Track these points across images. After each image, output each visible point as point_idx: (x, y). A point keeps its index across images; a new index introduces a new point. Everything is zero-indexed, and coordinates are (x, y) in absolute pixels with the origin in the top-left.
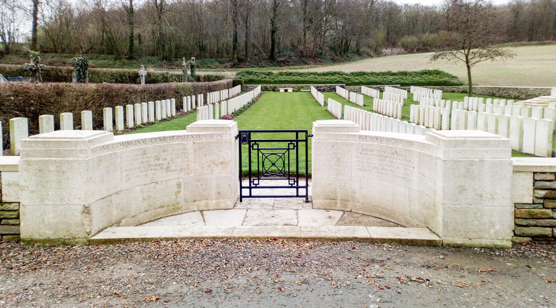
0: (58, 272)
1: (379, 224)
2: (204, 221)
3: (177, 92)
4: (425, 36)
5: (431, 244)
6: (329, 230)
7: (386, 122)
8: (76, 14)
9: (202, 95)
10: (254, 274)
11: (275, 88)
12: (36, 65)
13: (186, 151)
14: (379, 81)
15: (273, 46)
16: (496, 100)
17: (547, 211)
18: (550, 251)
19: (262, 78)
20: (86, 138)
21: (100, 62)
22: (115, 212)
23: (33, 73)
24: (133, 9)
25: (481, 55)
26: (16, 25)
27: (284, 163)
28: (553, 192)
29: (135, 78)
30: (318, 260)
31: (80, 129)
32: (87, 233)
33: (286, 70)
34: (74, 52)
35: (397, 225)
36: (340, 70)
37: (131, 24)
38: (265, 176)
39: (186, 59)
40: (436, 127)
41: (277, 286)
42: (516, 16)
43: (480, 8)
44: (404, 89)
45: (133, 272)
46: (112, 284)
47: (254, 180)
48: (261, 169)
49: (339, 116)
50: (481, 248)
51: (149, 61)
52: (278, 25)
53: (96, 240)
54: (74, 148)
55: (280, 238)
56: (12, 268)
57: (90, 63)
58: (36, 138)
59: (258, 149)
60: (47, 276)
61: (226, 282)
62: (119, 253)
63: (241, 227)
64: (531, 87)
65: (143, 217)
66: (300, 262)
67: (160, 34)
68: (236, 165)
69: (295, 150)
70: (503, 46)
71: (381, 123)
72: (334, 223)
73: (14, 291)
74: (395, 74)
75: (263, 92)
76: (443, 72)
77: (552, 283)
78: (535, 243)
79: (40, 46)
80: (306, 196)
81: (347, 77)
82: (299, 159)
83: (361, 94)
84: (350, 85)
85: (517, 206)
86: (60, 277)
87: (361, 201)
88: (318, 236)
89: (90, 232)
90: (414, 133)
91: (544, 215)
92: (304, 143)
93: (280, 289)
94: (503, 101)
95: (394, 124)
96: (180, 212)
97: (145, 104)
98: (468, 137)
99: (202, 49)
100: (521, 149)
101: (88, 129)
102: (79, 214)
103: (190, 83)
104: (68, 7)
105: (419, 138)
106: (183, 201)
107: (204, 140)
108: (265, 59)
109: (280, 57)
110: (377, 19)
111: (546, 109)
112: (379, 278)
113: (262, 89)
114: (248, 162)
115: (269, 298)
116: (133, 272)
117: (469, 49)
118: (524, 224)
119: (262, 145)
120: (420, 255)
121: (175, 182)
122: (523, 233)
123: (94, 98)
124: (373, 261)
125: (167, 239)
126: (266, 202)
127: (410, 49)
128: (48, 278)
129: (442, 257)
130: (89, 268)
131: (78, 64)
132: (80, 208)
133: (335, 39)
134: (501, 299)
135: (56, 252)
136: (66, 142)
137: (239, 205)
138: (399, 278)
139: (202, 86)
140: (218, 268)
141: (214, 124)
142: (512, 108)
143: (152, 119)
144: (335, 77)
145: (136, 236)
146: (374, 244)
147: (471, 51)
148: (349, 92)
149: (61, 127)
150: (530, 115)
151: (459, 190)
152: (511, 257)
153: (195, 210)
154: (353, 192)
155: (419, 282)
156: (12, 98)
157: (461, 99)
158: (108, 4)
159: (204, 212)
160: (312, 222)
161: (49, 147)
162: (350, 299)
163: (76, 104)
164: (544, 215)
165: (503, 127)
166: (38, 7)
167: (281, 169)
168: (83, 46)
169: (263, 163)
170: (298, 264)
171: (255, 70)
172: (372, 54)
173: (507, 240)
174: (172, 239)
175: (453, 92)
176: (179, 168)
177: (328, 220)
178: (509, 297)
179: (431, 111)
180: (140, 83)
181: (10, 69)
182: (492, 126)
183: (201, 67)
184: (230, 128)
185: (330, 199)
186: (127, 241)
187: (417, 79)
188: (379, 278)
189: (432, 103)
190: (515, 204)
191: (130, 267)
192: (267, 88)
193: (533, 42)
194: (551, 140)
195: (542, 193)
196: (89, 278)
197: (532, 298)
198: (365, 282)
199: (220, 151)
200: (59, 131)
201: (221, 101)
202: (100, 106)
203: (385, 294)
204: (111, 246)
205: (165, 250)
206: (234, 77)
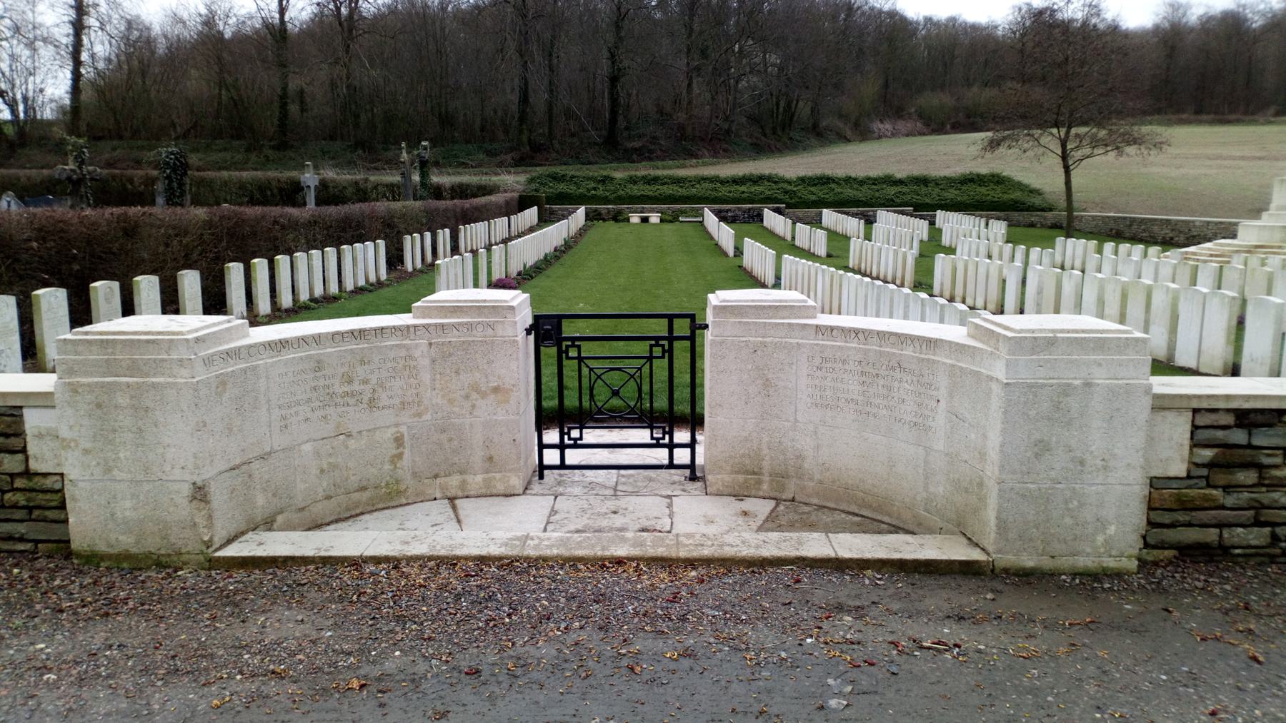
0: (153, 623)
1: (856, 528)
2: (459, 521)
3: (389, 225)
5: (967, 569)
6: (743, 542)
7: (879, 295)
8: (161, 48)
9: (447, 231)
10: (572, 637)
11: (620, 212)
12: (80, 168)
13: (412, 363)
14: (864, 198)
15: (614, 113)
16: (1124, 247)
17: (1214, 492)
18: (1212, 576)
19: (589, 191)
20: (189, 332)
21: (215, 157)
22: (260, 500)
23: (72, 187)
24: (285, 30)
25: (1095, 143)
26: (38, 81)
27: (640, 390)
28: (1228, 452)
29: (293, 193)
30: (717, 608)
31: (177, 312)
32: (204, 542)
33: (644, 170)
34: (157, 136)
35: (896, 529)
36: (774, 172)
37: (283, 65)
38: (597, 421)
39: (408, 146)
40: (991, 306)
41: (625, 662)
42: (1170, 56)
43: (1094, 34)
44: (921, 217)
45: (307, 628)
46: (265, 652)
47: (570, 429)
48: (586, 404)
49: (770, 280)
50: (1074, 575)
51: (324, 153)
52: (626, 63)
53: (224, 558)
54: (165, 357)
55: (631, 559)
56: (62, 611)
57: (193, 159)
58: (86, 333)
59: (580, 359)
60: (134, 631)
61: (511, 653)
62: (275, 587)
63: (542, 535)
65: (320, 510)
66: (675, 610)
67: (348, 87)
68: (527, 395)
69: (666, 360)
70: (1143, 124)
71: (866, 296)
72: (754, 526)
73: (70, 657)
74: (900, 182)
76: (1009, 179)
77: (1209, 642)
78: (1185, 562)
79: (88, 125)
80: (692, 466)
81: (789, 188)
82: (676, 381)
83: (822, 228)
84: (795, 206)
85: (1155, 483)
86: (156, 633)
87: (817, 476)
88: (716, 555)
89: (211, 540)
90: (942, 321)
91: (1207, 501)
92: (688, 343)
93: (632, 669)
95: (895, 300)
96: (404, 501)
97: (315, 253)
98: (1062, 331)
99: (447, 120)
100: (1171, 357)
101: (194, 312)
102: (185, 502)
103: (418, 203)
104: (145, 34)
105: (954, 332)
106: (409, 476)
107: (453, 337)
109: (630, 138)
110: (860, 50)
111: (1225, 270)
112: (852, 643)
113: (587, 215)
114: (556, 388)
115: (607, 687)
116: (307, 628)
117: (1070, 128)
118: (1167, 521)
119: (588, 349)
120: (944, 594)
121: (389, 434)
122: (1163, 542)
123: (204, 242)
124: (840, 608)
125: (377, 560)
126: (600, 480)
127: (937, 125)
128: (133, 633)
129: (990, 596)
130: (214, 618)
131: (168, 163)
132: (186, 490)
133: (761, 96)
134: (1106, 679)
135: (143, 582)
136: (148, 341)
137: (536, 487)
138: (895, 644)
139: (446, 210)
140: (491, 624)
141: (477, 299)
142: (1157, 265)
143: (334, 289)
144: (761, 189)
145: (309, 553)
146: (843, 572)
147: (1074, 131)
148: (794, 223)
149: (137, 309)
150: (1194, 282)
151: (1036, 449)
152: (1134, 592)
153: (438, 496)
154: (798, 457)
155: (939, 651)
156: (35, 244)
157: (1048, 243)
158: (230, 22)
159: (457, 502)
160: (702, 523)
161: (113, 353)
162: (786, 689)
163: (164, 254)
164: (1207, 501)
165: (1135, 310)
166: (84, 37)
167: (632, 404)
168: (176, 120)
169: (591, 389)
170: (670, 615)
171: (570, 170)
172: (849, 133)
173: (1129, 557)
174: (387, 559)
175: (1032, 225)
176: (397, 401)
177: (741, 520)
178: (1122, 674)
179: (982, 270)
180: (305, 204)
181: (29, 178)
182: (1113, 306)
183: (444, 166)
184: (512, 308)
185: (747, 472)
186: (289, 563)
187: (952, 194)
188: (852, 643)
189: (983, 251)
190: (1151, 479)
191: (299, 618)
192: (600, 214)
193: (1204, 117)
194: (1233, 337)
195: (1207, 454)
196: (215, 638)
197: (1165, 674)
198: (821, 653)
199: (490, 362)
200: (132, 317)
201: (491, 245)
202: (217, 258)
203: (864, 677)
204: (257, 572)
205: (374, 583)
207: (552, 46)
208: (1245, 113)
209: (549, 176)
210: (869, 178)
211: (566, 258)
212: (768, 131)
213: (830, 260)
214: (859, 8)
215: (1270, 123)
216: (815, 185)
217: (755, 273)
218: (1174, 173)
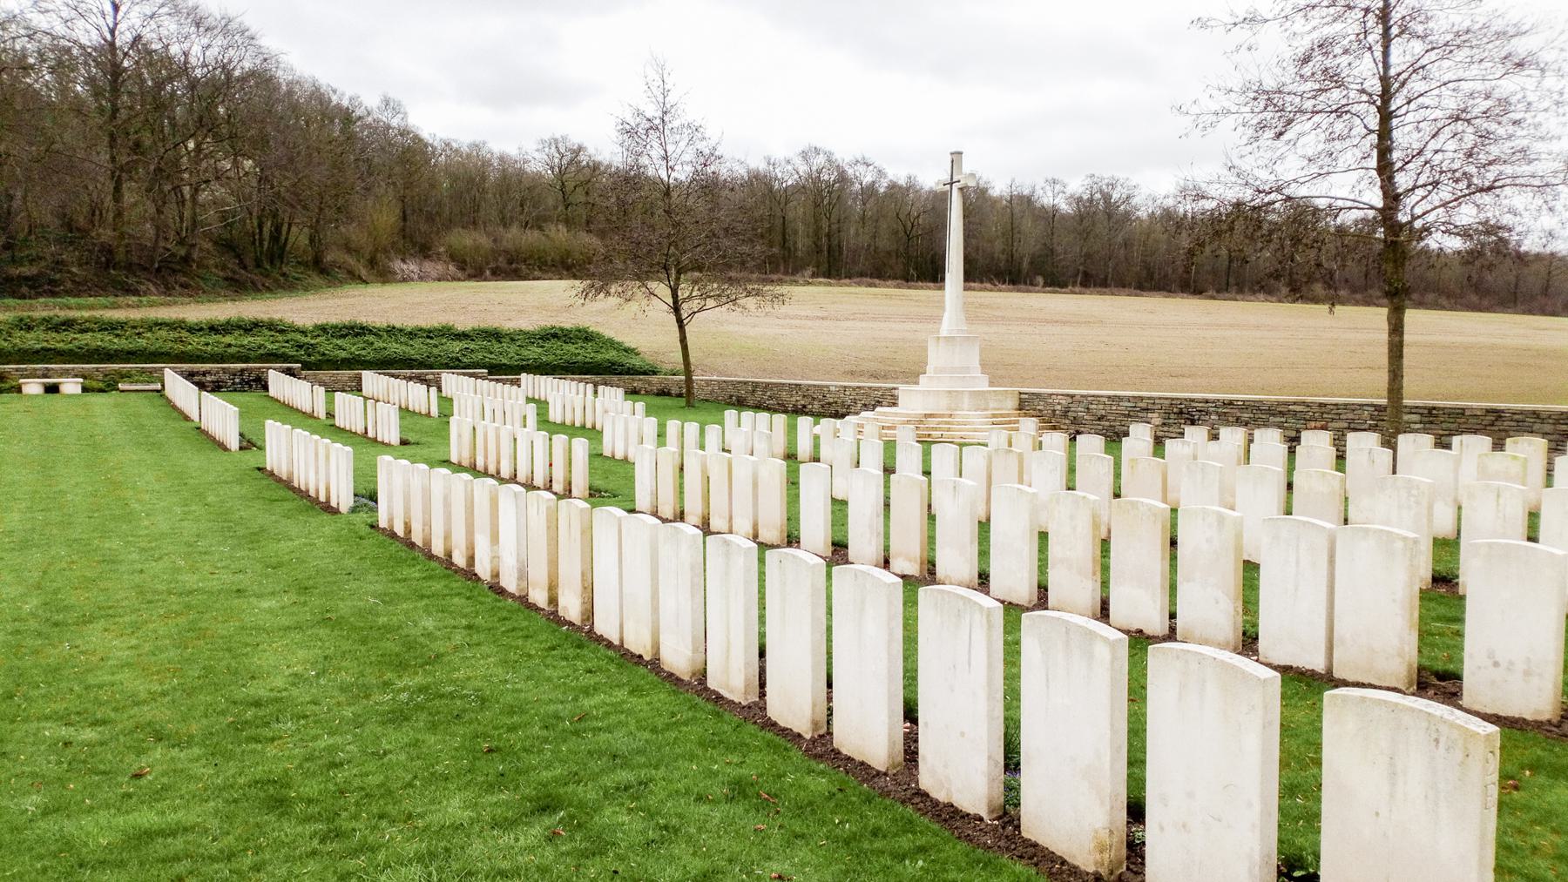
16: (747, 415)
33: (43, 308)
36: (277, 317)
64: (834, 384)
74: (463, 336)
81: (308, 340)
84: (318, 366)
94: (763, 416)
100: (1330, 671)
127: (473, 268)
144: (259, 340)
172: (364, 273)
187: (533, 352)
208: (786, 273)
213: (408, 450)
214: (360, 118)
216: (343, 336)
217: (300, 480)
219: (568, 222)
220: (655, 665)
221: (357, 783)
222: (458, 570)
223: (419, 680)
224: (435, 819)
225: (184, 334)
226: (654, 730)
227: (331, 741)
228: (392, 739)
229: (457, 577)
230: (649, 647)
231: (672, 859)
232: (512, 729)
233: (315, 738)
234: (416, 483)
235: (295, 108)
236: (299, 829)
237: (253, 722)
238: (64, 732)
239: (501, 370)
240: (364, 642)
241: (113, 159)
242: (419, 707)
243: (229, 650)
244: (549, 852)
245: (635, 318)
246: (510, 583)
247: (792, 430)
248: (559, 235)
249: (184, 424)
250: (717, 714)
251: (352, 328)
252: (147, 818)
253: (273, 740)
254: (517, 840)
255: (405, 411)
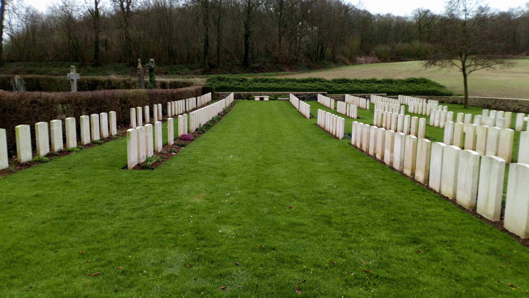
4: (398, 46)
11: (250, 95)
16: (493, 112)
19: (235, 85)
36: (321, 77)
74: (380, 82)
75: (236, 100)
76: (429, 81)
81: (330, 84)
99: (172, 54)
108: (238, 65)
109: (253, 62)
113: (235, 96)
127: (384, 58)
144: (316, 85)
171: (227, 76)
172: (347, 62)
187: (404, 87)
192: (240, 96)
206: (203, 84)
207: (219, 21)
208: (514, 54)
209: (217, 78)
210: (365, 80)
211: (224, 119)
212: (314, 60)
214: (351, 9)
215: (524, 58)
216: (340, 83)
218: (496, 79)
219: (420, 39)
220: (454, 201)
221: (351, 221)
222: (378, 160)
223: (368, 193)
224: (377, 237)
225: (296, 83)
226: (455, 224)
227: (342, 207)
228: (361, 210)
229: (378, 162)
230: (452, 194)
231: (465, 269)
232: (401, 214)
233: (338, 206)
234: (365, 130)
235: (331, 8)
236: (335, 231)
237: (320, 198)
238: (271, 193)
239: (392, 94)
240: (350, 179)
241: (279, 30)
242: (369, 202)
243: (311, 176)
244: (417, 257)
245: (447, 75)
246: (397, 166)
247: (514, 119)
248: (417, 44)
249: (295, 110)
250: (482, 223)
251: (343, 80)
252: (294, 219)
253: (325, 204)
254: (405, 250)
255: (359, 108)
